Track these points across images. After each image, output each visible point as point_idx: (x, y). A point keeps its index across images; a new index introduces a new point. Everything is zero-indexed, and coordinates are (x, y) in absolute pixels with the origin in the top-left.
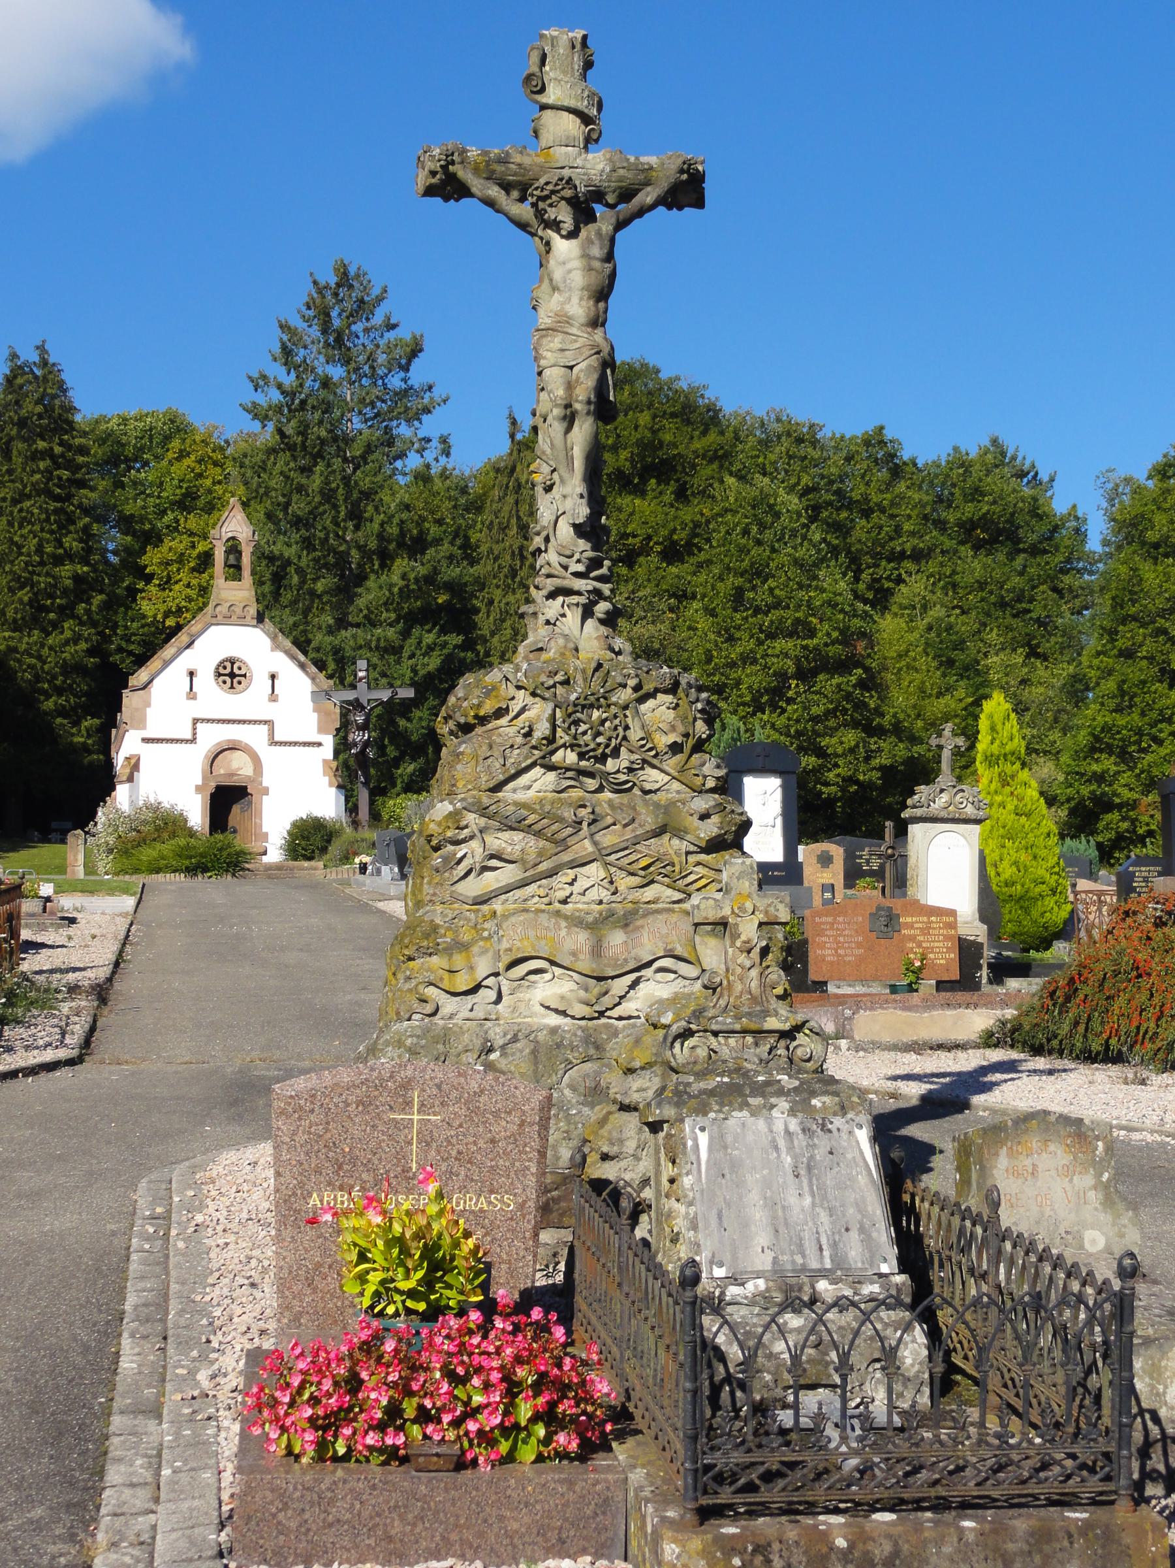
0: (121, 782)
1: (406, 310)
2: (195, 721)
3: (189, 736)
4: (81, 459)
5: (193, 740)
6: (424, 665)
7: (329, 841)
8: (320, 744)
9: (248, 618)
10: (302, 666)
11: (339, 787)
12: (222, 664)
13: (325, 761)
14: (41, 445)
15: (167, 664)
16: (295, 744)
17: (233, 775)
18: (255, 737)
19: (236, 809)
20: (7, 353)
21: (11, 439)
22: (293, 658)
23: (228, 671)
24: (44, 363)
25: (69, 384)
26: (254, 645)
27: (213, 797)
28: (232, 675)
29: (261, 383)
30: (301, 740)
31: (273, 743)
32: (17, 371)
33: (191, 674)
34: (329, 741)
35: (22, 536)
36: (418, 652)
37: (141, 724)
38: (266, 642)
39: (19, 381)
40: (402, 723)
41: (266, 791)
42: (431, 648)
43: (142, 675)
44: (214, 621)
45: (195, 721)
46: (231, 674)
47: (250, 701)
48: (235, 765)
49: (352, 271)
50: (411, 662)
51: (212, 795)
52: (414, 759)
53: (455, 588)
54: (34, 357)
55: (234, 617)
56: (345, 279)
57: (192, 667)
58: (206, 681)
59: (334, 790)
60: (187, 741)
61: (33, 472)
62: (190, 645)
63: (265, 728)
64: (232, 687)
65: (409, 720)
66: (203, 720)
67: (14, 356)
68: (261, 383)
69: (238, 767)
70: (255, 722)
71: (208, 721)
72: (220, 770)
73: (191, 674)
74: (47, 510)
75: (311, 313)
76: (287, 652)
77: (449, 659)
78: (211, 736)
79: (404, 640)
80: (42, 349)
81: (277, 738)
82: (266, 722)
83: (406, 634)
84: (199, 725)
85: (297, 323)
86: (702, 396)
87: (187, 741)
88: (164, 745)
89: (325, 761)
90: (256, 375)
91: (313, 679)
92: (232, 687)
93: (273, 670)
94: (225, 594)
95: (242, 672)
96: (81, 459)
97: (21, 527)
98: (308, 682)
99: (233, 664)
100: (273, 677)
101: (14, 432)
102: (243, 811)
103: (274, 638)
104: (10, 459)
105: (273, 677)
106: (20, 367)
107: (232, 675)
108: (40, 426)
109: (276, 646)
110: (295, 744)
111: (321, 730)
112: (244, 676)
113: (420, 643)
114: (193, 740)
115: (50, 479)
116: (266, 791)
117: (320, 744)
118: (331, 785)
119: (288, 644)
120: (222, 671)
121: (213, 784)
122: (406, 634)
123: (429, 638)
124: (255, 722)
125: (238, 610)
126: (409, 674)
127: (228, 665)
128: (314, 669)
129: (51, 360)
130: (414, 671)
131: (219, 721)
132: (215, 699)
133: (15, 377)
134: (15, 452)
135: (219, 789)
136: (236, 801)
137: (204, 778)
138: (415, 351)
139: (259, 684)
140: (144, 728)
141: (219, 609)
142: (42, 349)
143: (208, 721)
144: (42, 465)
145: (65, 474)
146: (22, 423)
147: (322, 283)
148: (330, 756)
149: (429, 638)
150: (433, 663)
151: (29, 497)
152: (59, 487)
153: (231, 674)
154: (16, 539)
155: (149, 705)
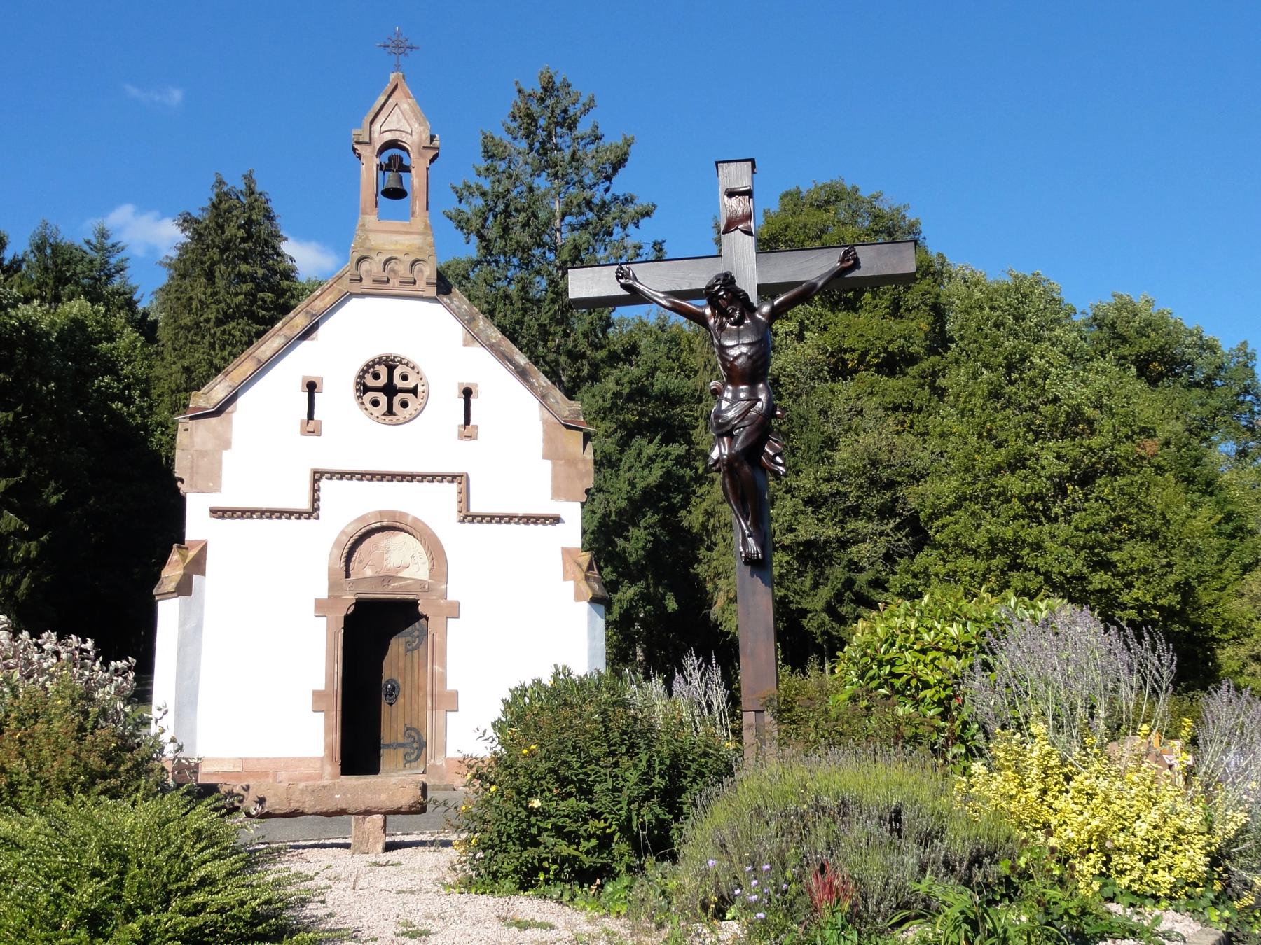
0: (166, 595)
1: (609, 122)
2: (318, 476)
3: (305, 505)
4: (285, 284)
5: (312, 513)
6: (643, 478)
7: (672, 798)
8: (556, 520)
9: (421, 284)
10: (522, 374)
11: (595, 600)
12: (369, 368)
13: (566, 552)
14: (244, 268)
15: (264, 367)
16: (510, 519)
17: (389, 578)
18: (432, 506)
19: (397, 645)
20: (213, 180)
21: (214, 264)
22: (505, 358)
23: (383, 381)
24: (251, 192)
25: (276, 212)
26: (437, 340)
27: (352, 623)
28: (390, 390)
29: (466, 193)
30: (521, 511)
31: (469, 517)
32: (222, 196)
33: (311, 387)
34: (572, 513)
35: (223, 358)
36: (637, 464)
37: (212, 482)
38: (456, 330)
39: (224, 206)
40: (620, 543)
41: (454, 611)
42: (651, 460)
43: (218, 390)
44: (356, 288)
45: (318, 476)
46: (387, 387)
47: (425, 438)
48: (393, 561)
49: (558, 81)
50: (628, 475)
51: (348, 619)
52: (633, 582)
53: (669, 399)
54: (241, 186)
55: (394, 282)
56: (549, 89)
57: (312, 374)
58: (339, 398)
59: (585, 606)
60: (300, 514)
61: (237, 294)
62: (307, 334)
63: (453, 488)
64: (390, 411)
65: (627, 539)
66: (332, 475)
67: (221, 183)
68: (466, 193)
69: (401, 562)
70: (433, 478)
71: (342, 475)
72: (365, 568)
73: (311, 387)
74: (249, 332)
75: (515, 124)
76: (493, 348)
77: (668, 474)
78: (347, 506)
79: (621, 452)
80: (249, 179)
81: (475, 508)
82: (453, 478)
83: (624, 444)
84: (324, 484)
85: (501, 135)
86: (904, 217)
87: (300, 514)
88: (255, 523)
89: (566, 552)
90: (460, 186)
91: (543, 398)
92: (390, 411)
93: (468, 381)
94: (376, 240)
95: (410, 384)
96: (285, 284)
97: (222, 349)
98: (534, 403)
99: (391, 369)
100: (467, 393)
101: (216, 257)
102: (409, 650)
103: (468, 323)
104: (214, 283)
105: (467, 393)
106: (226, 194)
107: (390, 390)
108: (244, 250)
109: (474, 337)
110: (510, 519)
111: (558, 492)
112: (414, 391)
113: (639, 454)
114: (312, 513)
115: (253, 302)
116: (454, 611)
117: (556, 520)
118: (578, 597)
119: (496, 335)
120: (370, 381)
121: (350, 598)
122: (624, 444)
123: (650, 450)
124: (433, 478)
125: (402, 269)
126: (626, 487)
127: (383, 371)
128: (543, 381)
129: (258, 189)
130: (632, 484)
131: (363, 476)
132: (354, 433)
133: (221, 202)
134: (217, 274)
135: (360, 604)
136: (397, 630)
137: (333, 586)
138: (620, 163)
139: (442, 407)
140: (217, 488)
141: (365, 266)
142: (249, 179)
143: (342, 475)
144: (245, 288)
145: (269, 296)
146: (226, 247)
147: (528, 91)
148: (576, 541)
149: (650, 450)
150: (654, 476)
151: (233, 319)
152: (263, 309)
153: (387, 387)
154: (216, 361)
155: (227, 445)
